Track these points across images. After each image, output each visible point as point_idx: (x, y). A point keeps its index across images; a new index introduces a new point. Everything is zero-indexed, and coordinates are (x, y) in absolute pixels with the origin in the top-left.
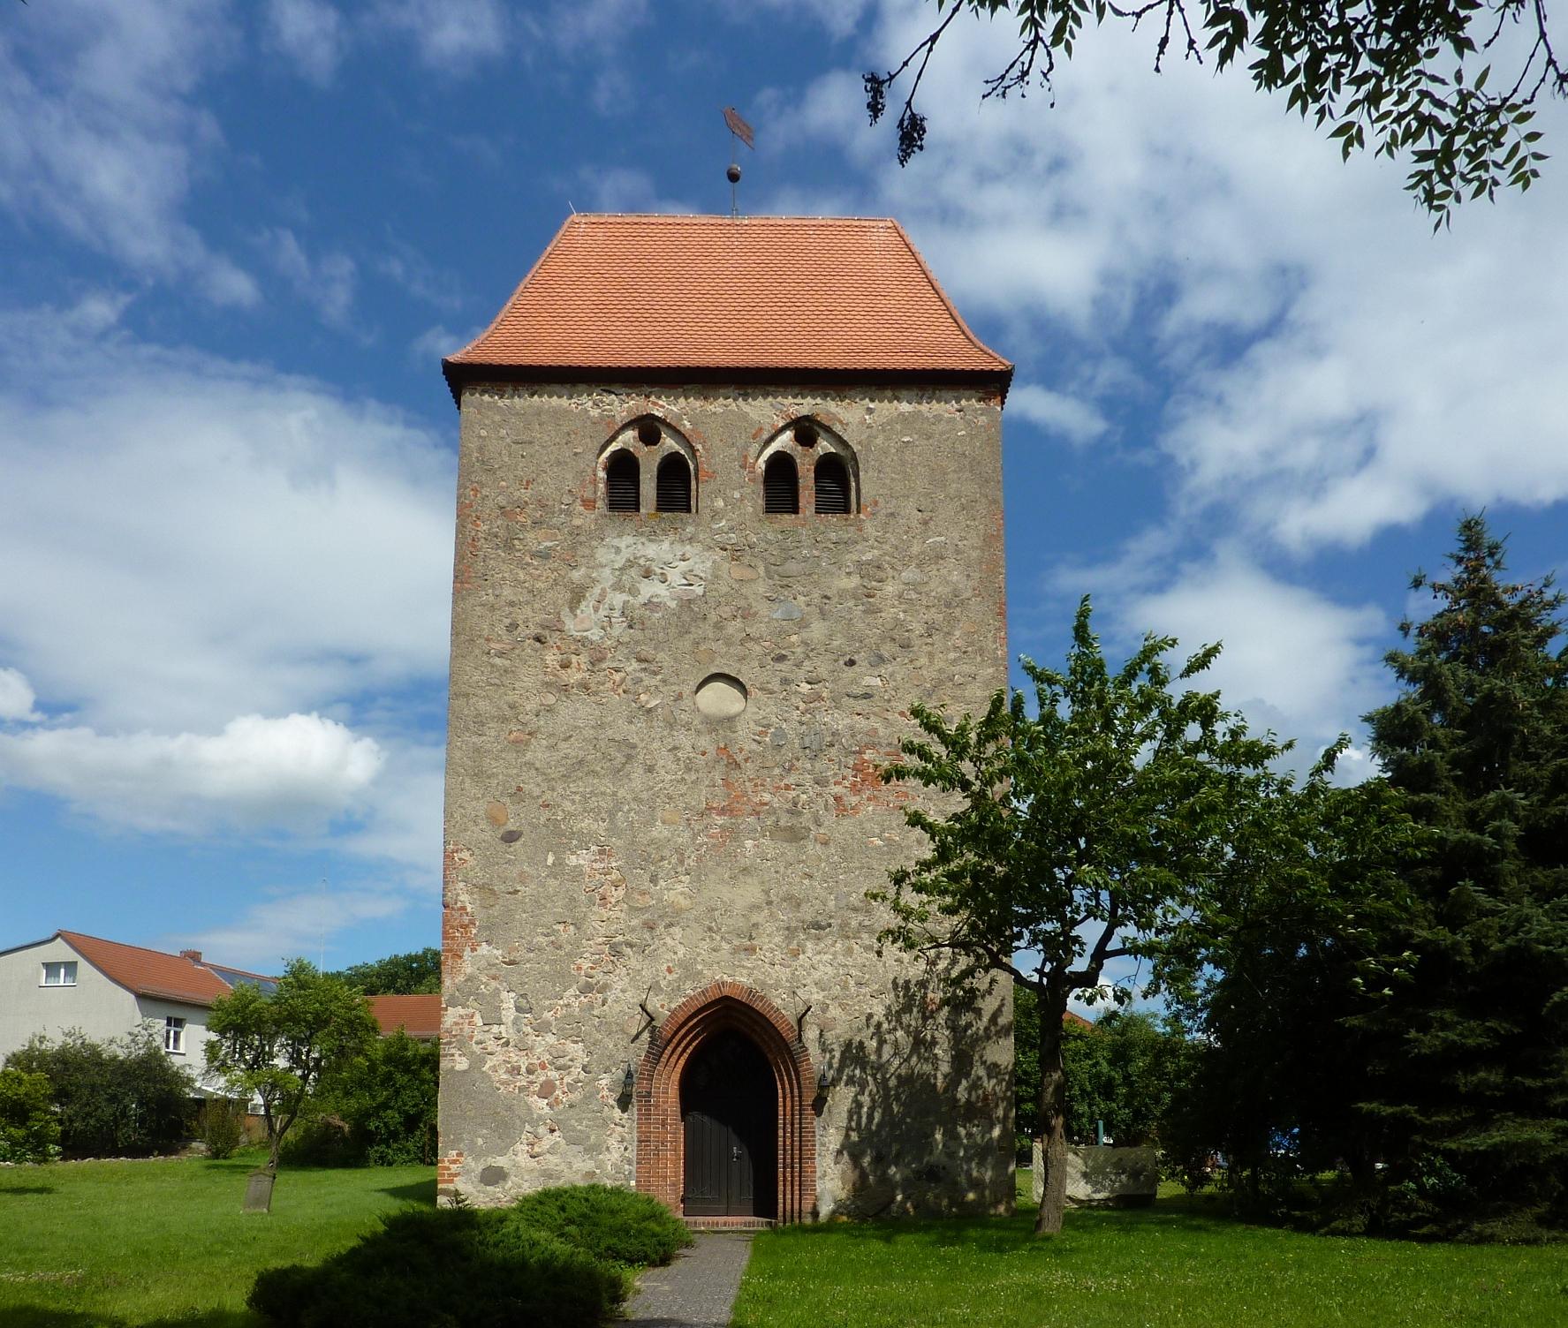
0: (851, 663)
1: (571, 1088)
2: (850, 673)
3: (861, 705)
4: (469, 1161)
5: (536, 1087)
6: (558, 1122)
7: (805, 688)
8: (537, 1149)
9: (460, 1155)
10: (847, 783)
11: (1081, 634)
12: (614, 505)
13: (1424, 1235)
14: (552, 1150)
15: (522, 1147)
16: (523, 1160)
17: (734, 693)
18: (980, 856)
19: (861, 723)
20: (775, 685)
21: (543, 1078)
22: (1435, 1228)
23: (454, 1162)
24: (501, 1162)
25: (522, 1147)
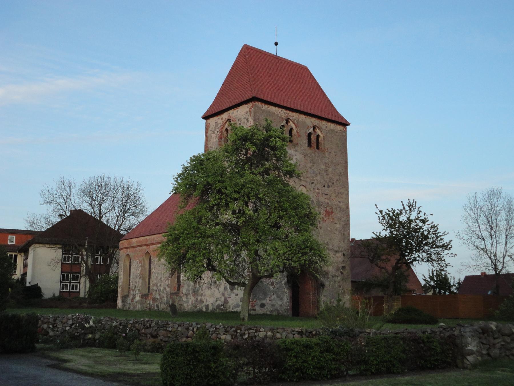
0: (324, 186)
1: (277, 283)
2: (324, 189)
3: (326, 196)
4: (258, 301)
5: (270, 283)
6: (276, 292)
7: (317, 191)
8: (271, 299)
9: (256, 300)
10: (324, 214)
11: (450, 241)
12: (308, 146)
13: (231, 282)
14: (274, 299)
15: (268, 298)
16: (268, 301)
17: (304, 188)
18: (285, 212)
19: (327, 201)
20: (312, 189)
21: (272, 281)
22: (444, 325)
23: (255, 302)
24: (264, 302)
25: (268, 298)
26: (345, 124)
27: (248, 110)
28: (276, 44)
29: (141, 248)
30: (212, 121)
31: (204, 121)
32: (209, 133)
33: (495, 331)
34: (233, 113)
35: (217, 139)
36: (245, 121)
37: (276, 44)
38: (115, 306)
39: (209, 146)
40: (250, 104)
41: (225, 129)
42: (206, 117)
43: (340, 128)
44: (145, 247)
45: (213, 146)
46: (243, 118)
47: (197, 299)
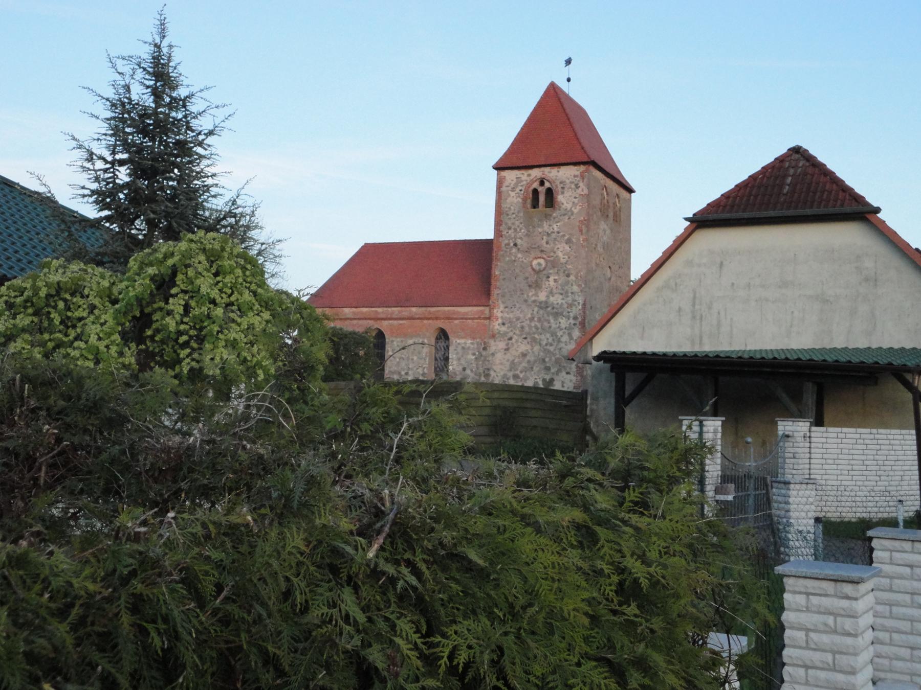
26: (630, 190)
27: (578, 173)
28: (569, 80)
29: (361, 322)
30: (511, 176)
31: (496, 172)
32: (504, 189)
33: (208, 397)
34: (550, 172)
35: (520, 200)
36: (573, 186)
37: (569, 80)
38: (22, 375)
39: (504, 206)
40: (582, 168)
41: (532, 188)
42: (499, 168)
43: (624, 193)
44: (372, 321)
45: (512, 208)
46: (568, 181)
47: (78, 359)
